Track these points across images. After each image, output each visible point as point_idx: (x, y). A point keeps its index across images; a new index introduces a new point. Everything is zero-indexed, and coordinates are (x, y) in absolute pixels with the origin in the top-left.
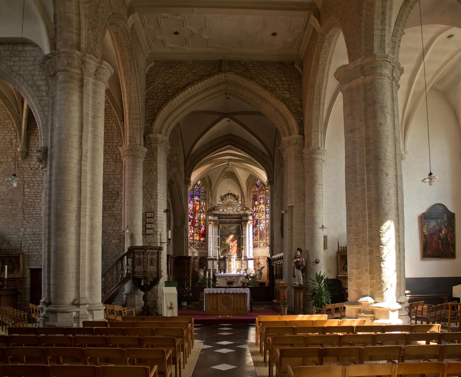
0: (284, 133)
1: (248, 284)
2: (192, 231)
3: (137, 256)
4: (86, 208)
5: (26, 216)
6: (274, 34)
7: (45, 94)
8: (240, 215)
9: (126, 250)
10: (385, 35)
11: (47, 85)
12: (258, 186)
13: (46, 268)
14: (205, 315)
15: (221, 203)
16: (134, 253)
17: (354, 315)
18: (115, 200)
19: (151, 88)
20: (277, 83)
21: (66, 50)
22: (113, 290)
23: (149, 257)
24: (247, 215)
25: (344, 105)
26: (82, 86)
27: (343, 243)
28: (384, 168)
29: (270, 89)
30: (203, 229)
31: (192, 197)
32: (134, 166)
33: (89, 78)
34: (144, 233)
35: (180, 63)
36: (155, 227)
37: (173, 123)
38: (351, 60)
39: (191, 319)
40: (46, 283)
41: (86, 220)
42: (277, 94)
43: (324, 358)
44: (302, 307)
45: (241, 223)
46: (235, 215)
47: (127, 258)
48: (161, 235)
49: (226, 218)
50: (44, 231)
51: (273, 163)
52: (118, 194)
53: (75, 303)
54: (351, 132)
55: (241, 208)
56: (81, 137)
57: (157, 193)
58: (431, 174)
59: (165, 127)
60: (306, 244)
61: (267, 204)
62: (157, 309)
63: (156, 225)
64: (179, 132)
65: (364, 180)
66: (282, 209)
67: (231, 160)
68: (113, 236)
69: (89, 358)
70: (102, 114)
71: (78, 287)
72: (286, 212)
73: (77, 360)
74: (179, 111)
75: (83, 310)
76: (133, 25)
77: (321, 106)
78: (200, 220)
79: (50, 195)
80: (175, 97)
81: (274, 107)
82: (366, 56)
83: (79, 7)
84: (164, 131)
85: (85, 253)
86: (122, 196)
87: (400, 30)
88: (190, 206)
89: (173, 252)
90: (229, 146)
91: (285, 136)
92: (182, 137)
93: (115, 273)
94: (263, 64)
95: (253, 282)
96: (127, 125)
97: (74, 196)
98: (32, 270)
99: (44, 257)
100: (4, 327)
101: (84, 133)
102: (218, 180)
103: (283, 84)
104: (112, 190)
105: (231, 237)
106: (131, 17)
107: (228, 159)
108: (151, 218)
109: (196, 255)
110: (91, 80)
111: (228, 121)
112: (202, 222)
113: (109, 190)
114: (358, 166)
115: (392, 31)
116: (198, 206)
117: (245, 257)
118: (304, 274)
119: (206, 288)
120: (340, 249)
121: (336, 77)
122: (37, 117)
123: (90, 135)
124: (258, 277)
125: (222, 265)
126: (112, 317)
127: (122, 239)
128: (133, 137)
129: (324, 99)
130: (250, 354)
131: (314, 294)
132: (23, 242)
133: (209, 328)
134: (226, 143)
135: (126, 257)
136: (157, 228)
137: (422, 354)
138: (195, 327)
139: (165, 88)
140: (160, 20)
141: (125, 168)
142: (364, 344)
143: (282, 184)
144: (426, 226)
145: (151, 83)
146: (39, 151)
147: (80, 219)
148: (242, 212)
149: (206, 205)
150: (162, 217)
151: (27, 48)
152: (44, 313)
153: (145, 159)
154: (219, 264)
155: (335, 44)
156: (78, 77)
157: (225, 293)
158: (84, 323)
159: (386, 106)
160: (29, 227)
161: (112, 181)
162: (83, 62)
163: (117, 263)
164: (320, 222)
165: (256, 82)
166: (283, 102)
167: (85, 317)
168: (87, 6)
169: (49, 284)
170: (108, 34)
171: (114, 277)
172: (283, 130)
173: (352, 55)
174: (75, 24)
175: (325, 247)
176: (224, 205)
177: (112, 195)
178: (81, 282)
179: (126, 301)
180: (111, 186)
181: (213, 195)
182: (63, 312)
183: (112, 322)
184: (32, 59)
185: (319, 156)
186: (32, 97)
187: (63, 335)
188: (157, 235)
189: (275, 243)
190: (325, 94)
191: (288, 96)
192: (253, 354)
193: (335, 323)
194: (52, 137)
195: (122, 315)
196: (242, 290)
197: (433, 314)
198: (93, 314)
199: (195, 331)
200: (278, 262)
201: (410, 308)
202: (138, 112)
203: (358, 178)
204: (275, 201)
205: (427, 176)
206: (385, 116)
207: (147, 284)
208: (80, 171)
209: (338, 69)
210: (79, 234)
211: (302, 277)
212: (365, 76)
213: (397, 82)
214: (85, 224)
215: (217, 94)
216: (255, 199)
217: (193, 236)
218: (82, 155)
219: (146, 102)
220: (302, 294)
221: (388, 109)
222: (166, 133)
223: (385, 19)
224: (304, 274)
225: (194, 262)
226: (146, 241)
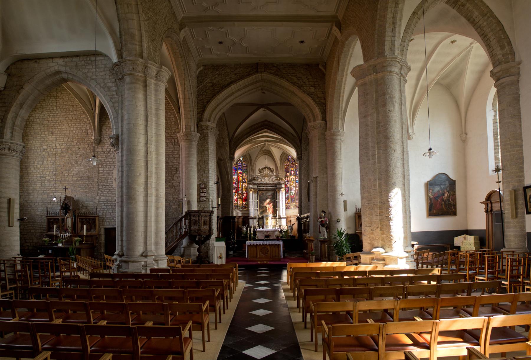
0: (310, 120)
1: (282, 237)
3: (193, 218)
4: (152, 182)
5: (100, 187)
6: (302, 42)
7: (115, 93)
8: (275, 184)
9: (184, 214)
10: (395, 41)
11: (117, 86)
12: (289, 161)
13: (120, 228)
14: (247, 261)
16: (190, 216)
17: (368, 262)
20: (304, 81)
21: (131, 58)
23: (203, 219)
24: (280, 184)
25: (359, 97)
26: (145, 86)
27: (359, 206)
28: (392, 146)
30: (245, 195)
31: (236, 170)
32: (189, 148)
35: (225, 66)
37: (220, 113)
38: (366, 60)
39: (236, 265)
40: (120, 239)
41: (152, 191)
47: (185, 220)
48: (212, 202)
50: (117, 198)
51: (301, 143)
53: (144, 255)
56: (146, 126)
57: (208, 169)
58: (430, 149)
59: (213, 116)
61: (296, 175)
62: (209, 258)
63: (209, 193)
65: (375, 155)
66: (308, 179)
67: (267, 141)
70: (163, 107)
71: (146, 243)
72: (312, 181)
73: (146, 298)
74: (224, 103)
75: (150, 260)
78: (242, 188)
79: (122, 172)
81: (302, 100)
82: (378, 57)
83: (140, 24)
84: (212, 119)
87: (408, 37)
88: (235, 177)
92: (226, 124)
93: (175, 231)
94: (292, 66)
95: (286, 235)
96: (183, 116)
97: (141, 172)
98: (106, 229)
99: (118, 219)
100: (85, 272)
101: (149, 123)
102: (257, 156)
103: (309, 82)
105: (268, 201)
106: (182, 31)
108: (204, 188)
109: (240, 215)
110: (153, 81)
112: (244, 190)
114: (370, 144)
115: (401, 37)
117: (279, 216)
119: (247, 240)
122: (109, 111)
124: (289, 231)
125: (261, 223)
126: (172, 265)
127: (180, 205)
129: (343, 93)
130: (282, 291)
131: (337, 246)
132: (98, 208)
133: (251, 272)
136: (209, 196)
137: (425, 292)
138: (239, 270)
139: (212, 86)
142: (376, 284)
143: (308, 160)
144: (431, 191)
145: (201, 82)
146: (112, 138)
148: (276, 182)
150: (213, 188)
151: (98, 58)
152: (118, 262)
155: (353, 48)
156: (142, 79)
157: (263, 245)
158: (151, 270)
159: (395, 97)
160: (103, 196)
162: (146, 67)
164: (340, 189)
168: (146, 23)
169: (122, 241)
170: (164, 45)
173: (366, 57)
174: (137, 38)
175: (345, 209)
177: (172, 171)
178: (148, 239)
179: (184, 253)
181: (253, 169)
182: (133, 262)
183: (174, 269)
184: (103, 66)
185: (339, 137)
187: (134, 279)
188: (209, 201)
189: (303, 206)
190: (344, 88)
192: (285, 290)
193: (352, 268)
194: (122, 126)
195: (181, 263)
196: (276, 242)
197: (436, 260)
198: (158, 263)
199: (239, 274)
200: (305, 220)
201: (417, 254)
202: (191, 106)
203: (370, 153)
204: (303, 172)
205: (428, 151)
206: (393, 104)
207: (201, 239)
208: (147, 152)
209: (354, 68)
210: (146, 202)
211: (326, 233)
212: (377, 73)
213: (404, 78)
215: (255, 90)
216: (287, 171)
217: (237, 200)
219: (198, 96)
221: (397, 99)
223: (395, 27)
225: (238, 221)
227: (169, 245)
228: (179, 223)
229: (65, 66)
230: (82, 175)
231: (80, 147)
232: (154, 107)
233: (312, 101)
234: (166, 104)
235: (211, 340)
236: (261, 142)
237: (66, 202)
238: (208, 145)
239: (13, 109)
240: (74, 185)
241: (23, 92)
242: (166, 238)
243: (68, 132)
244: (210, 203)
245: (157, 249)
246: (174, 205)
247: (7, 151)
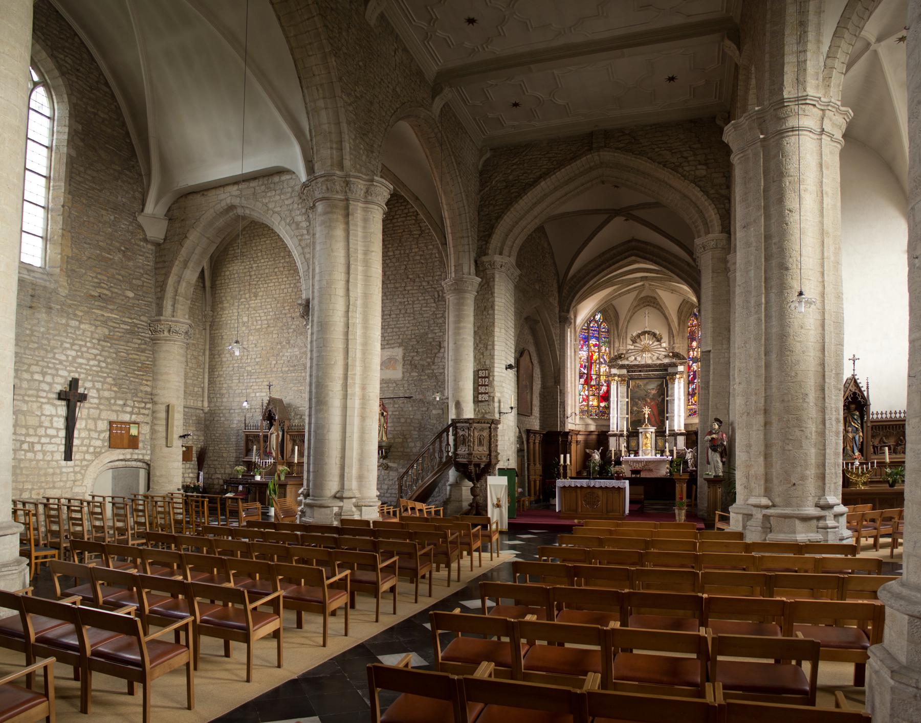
2: (586, 393)
3: (461, 433)
6: (671, 79)
7: (305, 232)
11: (308, 220)
15: (632, 347)
19: (487, 189)
20: (685, 154)
23: (476, 434)
26: (347, 215)
29: (673, 165)
30: (604, 388)
32: (460, 305)
41: (356, 390)
48: (500, 402)
52: (440, 346)
56: (348, 281)
57: (493, 342)
63: (493, 387)
64: (546, 245)
67: (653, 279)
71: (342, 476)
75: (348, 505)
78: (599, 376)
84: (506, 252)
85: (353, 433)
90: (633, 258)
106: (437, 99)
108: (485, 377)
109: (592, 428)
112: (603, 379)
117: (671, 430)
125: (633, 444)
127: (445, 408)
134: (627, 254)
136: (493, 392)
139: (506, 187)
148: (666, 361)
153: (478, 292)
157: (589, 487)
162: (347, 183)
168: (351, 108)
172: (696, 227)
178: (346, 470)
179: (450, 495)
180: (430, 336)
186: (291, 238)
191: (704, 173)
194: (313, 285)
198: (361, 511)
208: (347, 326)
210: (345, 408)
211: (720, 464)
214: (353, 395)
219: (480, 210)
220: (719, 490)
229: (240, 196)
230: (296, 362)
231: (293, 315)
233: (700, 194)
236: (634, 281)
237: (270, 407)
238: (493, 297)
239: (175, 270)
240: (284, 380)
241: (188, 243)
243: (278, 292)
244: (496, 405)
245: (361, 487)
247: (166, 333)
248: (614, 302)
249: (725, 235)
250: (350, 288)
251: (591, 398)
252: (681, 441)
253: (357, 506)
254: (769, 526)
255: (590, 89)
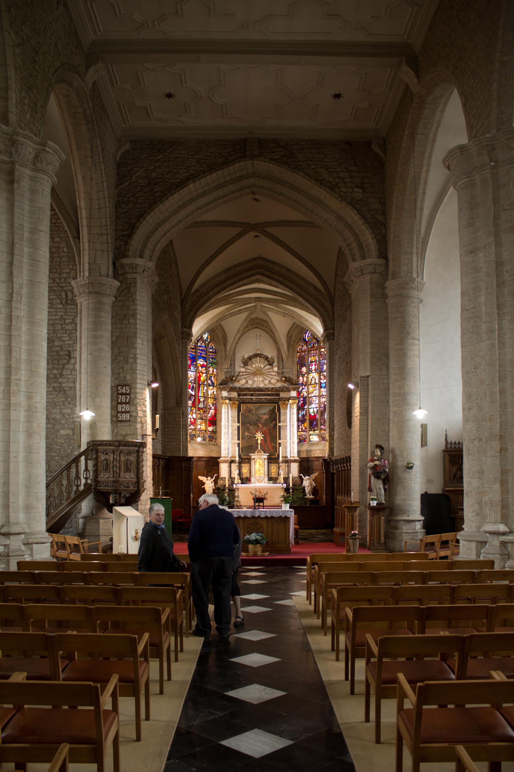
2: (194, 416)
3: (103, 457)
4: (19, 380)
6: (337, 96)
9: (83, 447)
12: (306, 343)
15: (244, 370)
16: (97, 451)
18: (64, 365)
19: (125, 184)
22: (62, 510)
23: (123, 458)
30: (212, 411)
31: (194, 359)
33: (23, 169)
34: (115, 419)
36: (133, 409)
42: (341, 194)
43: (428, 622)
44: (382, 538)
45: (278, 403)
46: (267, 389)
47: (86, 460)
49: (252, 395)
51: (333, 305)
52: (69, 356)
54: (471, 252)
55: (278, 378)
57: (135, 355)
59: (150, 246)
60: (391, 438)
63: (135, 406)
64: (172, 254)
67: (267, 301)
68: (61, 424)
69: (32, 620)
70: (45, 226)
76: (95, 82)
77: (418, 212)
78: (206, 397)
80: (167, 199)
84: (147, 253)
86: (76, 358)
88: (191, 375)
89: (163, 450)
90: (259, 277)
91: (354, 260)
93: (65, 482)
96: (85, 245)
101: (16, 258)
104: (58, 349)
106: (92, 69)
107: (256, 298)
110: (28, 172)
111: (257, 236)
113: (54, 349)
114: (484, 309)
116: (204, 375)
118: (386, 487)
120: (449, 446)
121: (447, 164)
123: (25, 260)
125: (245, 470)
126: (62, 554)
128: (94, 263)
129: (423, 201)
134: (252, 272)
135: (83, 458)
136: (136, 411)
140: (142, 75)
141: (81, 314)
143: (349, 341)
147: (10, 397)
149: (217, 373)
154: (240, 468)
155: (443, 111)
157: (253, 517)
158: (20, 564)
161: (59, 335)
162: (13, 143)
163: (68, 467)
165: (305, 174)
166: (352, 205)
167: (18, 553)
170: (53, 100)
171: (64, 489)
175: (424, 443)
176: (249, 374)
178: (12, 499)
179: (84, 529)
185: (415, 293)
188: (136, 422)
190: (424, 193)
198: (31, 550)
204: (337, 367)
211: (383, 492)
216: (302, 363)
218: (12, 293)
219: (118, 206)
220: (383, 518)
222: (151, 257)
224: (386, 487)
226: (117, 433)
227: (53, 512)
228: (74, 465)
232: (27, 226)
233: (357, 218)
234: (51, 219)
235: (152, 717)
242: (48, 498)
246: (63, 429)
248: (222, 323)
249: (381, 261)
250: (15, 273)
251: (199, 421)
252: (295, 468)
253: (27, 544)
254: (506, 552)
255: (249, 94)
